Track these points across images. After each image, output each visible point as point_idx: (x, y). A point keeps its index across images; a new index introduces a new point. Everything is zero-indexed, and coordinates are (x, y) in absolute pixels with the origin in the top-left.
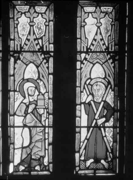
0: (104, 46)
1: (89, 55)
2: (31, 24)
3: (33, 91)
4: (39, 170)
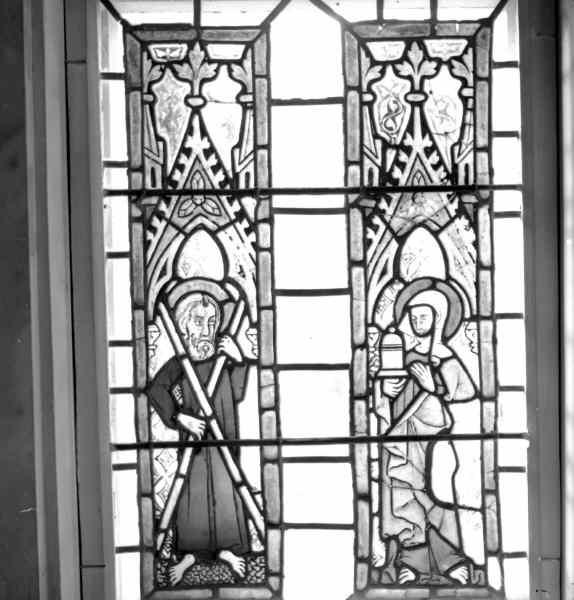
0: (220, 173)
1: (168, 202)
2: (421, 98)
3: (205, 323)
4: (464, 582)
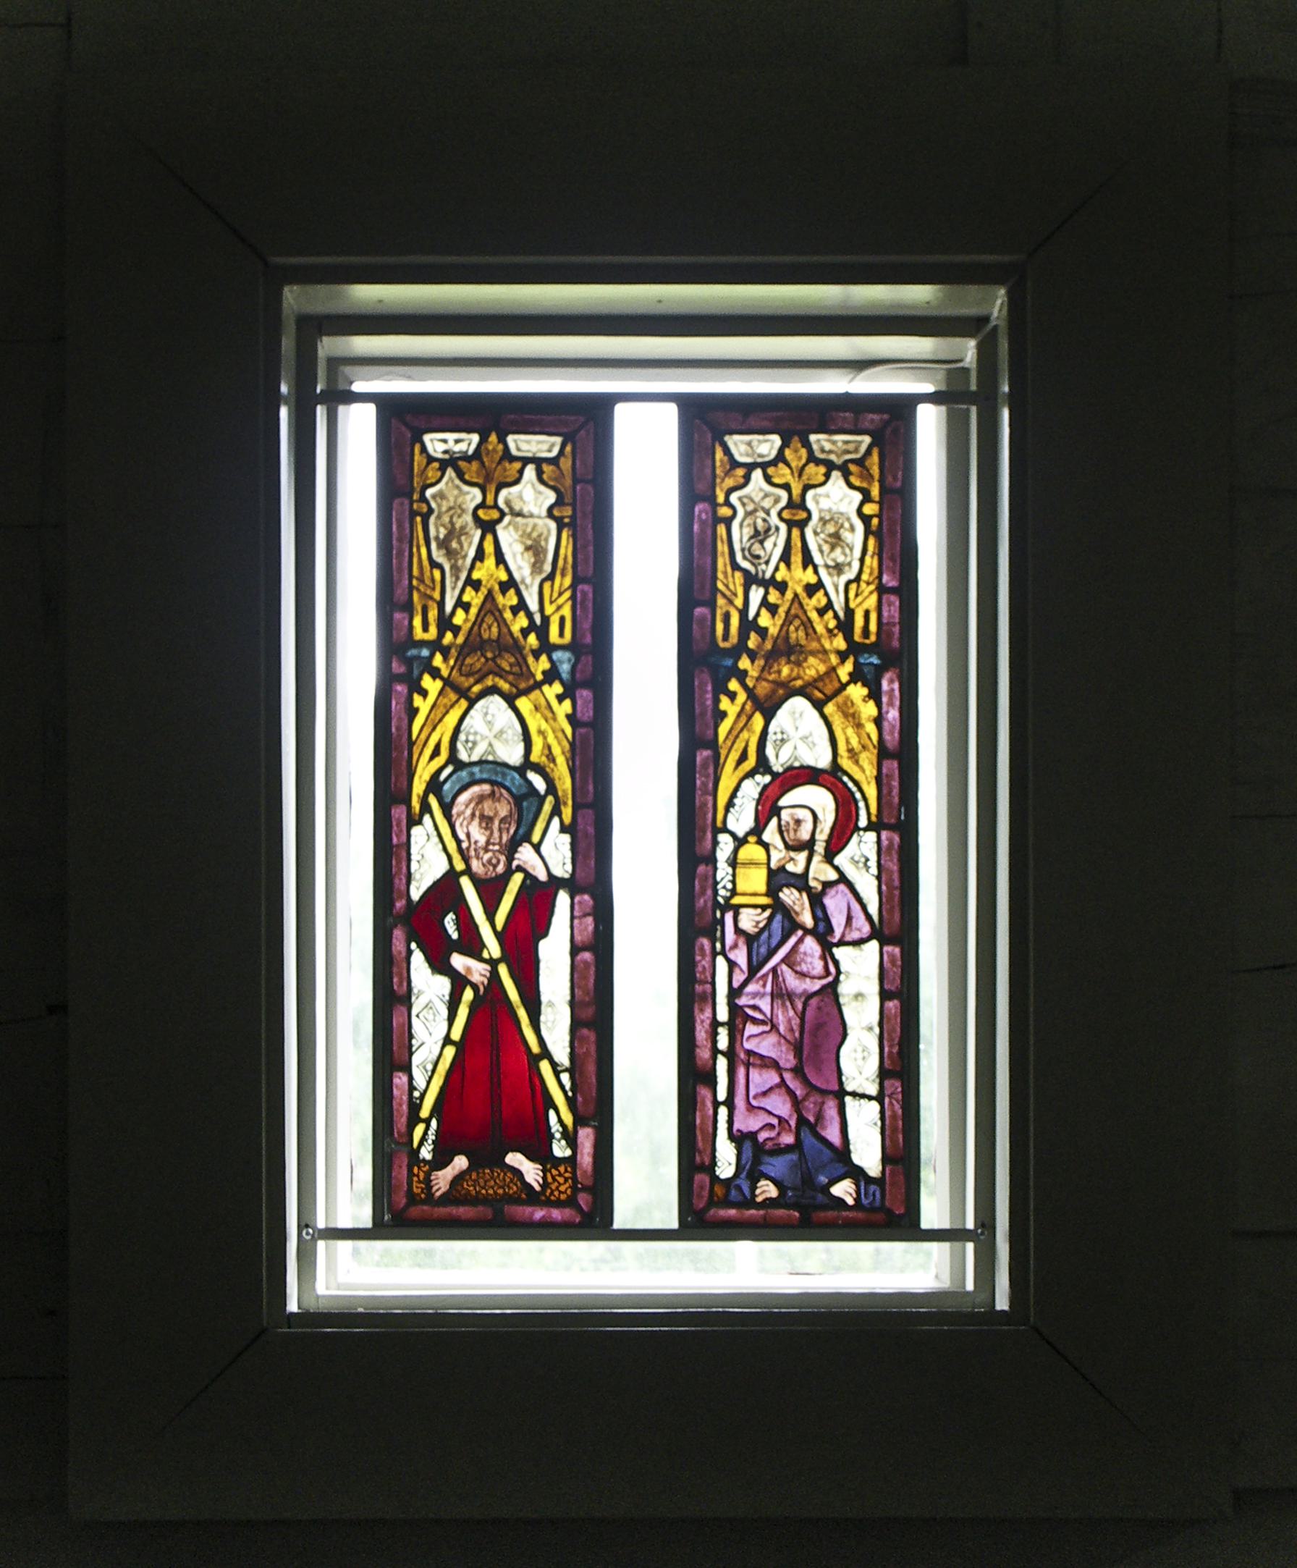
4: (850, 1201)
